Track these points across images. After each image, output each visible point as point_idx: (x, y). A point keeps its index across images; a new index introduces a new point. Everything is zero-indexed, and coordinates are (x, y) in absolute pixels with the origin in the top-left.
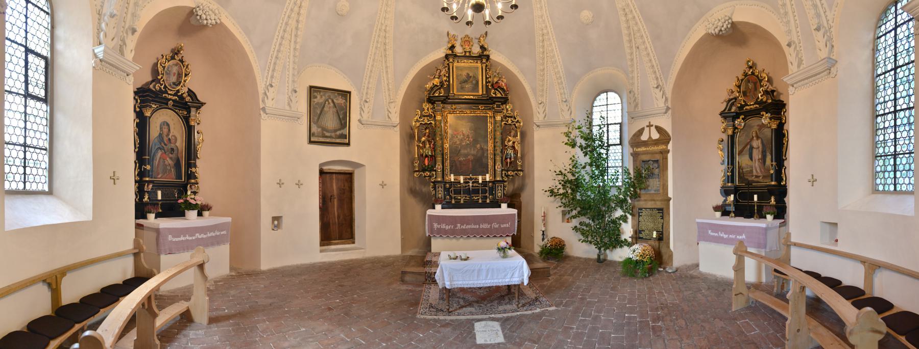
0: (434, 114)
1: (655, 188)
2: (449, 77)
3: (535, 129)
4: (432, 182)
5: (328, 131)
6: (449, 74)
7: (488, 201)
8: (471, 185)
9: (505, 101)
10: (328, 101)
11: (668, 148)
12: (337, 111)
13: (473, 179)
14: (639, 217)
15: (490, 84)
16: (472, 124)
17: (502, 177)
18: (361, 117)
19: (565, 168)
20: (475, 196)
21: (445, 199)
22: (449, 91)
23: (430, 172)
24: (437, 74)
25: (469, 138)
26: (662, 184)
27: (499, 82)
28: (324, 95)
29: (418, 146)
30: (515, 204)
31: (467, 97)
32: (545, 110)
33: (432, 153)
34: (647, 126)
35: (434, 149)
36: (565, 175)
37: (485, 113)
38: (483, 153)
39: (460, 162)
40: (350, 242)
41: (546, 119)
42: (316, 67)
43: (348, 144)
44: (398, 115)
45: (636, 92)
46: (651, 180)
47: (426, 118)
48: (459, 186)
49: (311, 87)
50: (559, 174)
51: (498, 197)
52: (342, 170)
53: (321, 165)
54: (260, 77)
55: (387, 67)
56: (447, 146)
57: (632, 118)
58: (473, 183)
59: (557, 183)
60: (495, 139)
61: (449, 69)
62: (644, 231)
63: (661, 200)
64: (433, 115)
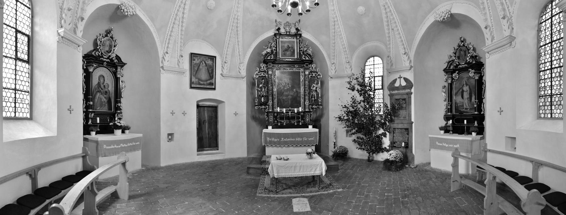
0: (267, 70)
2: (276, 47)
3: (329, 80)
4: (266, 112)
5: (202, 81)
7: (301, 124)
8: (290, 114)
9: (311, 62)
10: (202, 62)
12: (208, 68)
14: (393, 134)
15: (302, 52)
17: (309, 109)
19: (348, 104)
20: (293, 121)
21: (274, 122)
23: (265, 106)
24: (269, 46)
26: (407, 113)
28: (200, 59)
29: (258, 90)
32: (336, 68)
33: (266, 94)
34: (399, 78)
36: (348, 108)
37: (299, 70)
38: (298, 94)
39: (283, 99)
40: (216, 149)
43: (214, 89)
44: (245, 70)
45: (392, 57)
46: (401, 111)
47: (262, 73)
48: (283, 114)
49: (191, 54)
50: (344, 107)
51: (307, 121)
52: (210, 105)
53: (198, 102)
54: (160, 47)
55: (238, 41)
56: (275, 90)
57: (390, 73)
58: (291, 113)
61: (276, 42)
63: (407, 124)
64: (267, 71)
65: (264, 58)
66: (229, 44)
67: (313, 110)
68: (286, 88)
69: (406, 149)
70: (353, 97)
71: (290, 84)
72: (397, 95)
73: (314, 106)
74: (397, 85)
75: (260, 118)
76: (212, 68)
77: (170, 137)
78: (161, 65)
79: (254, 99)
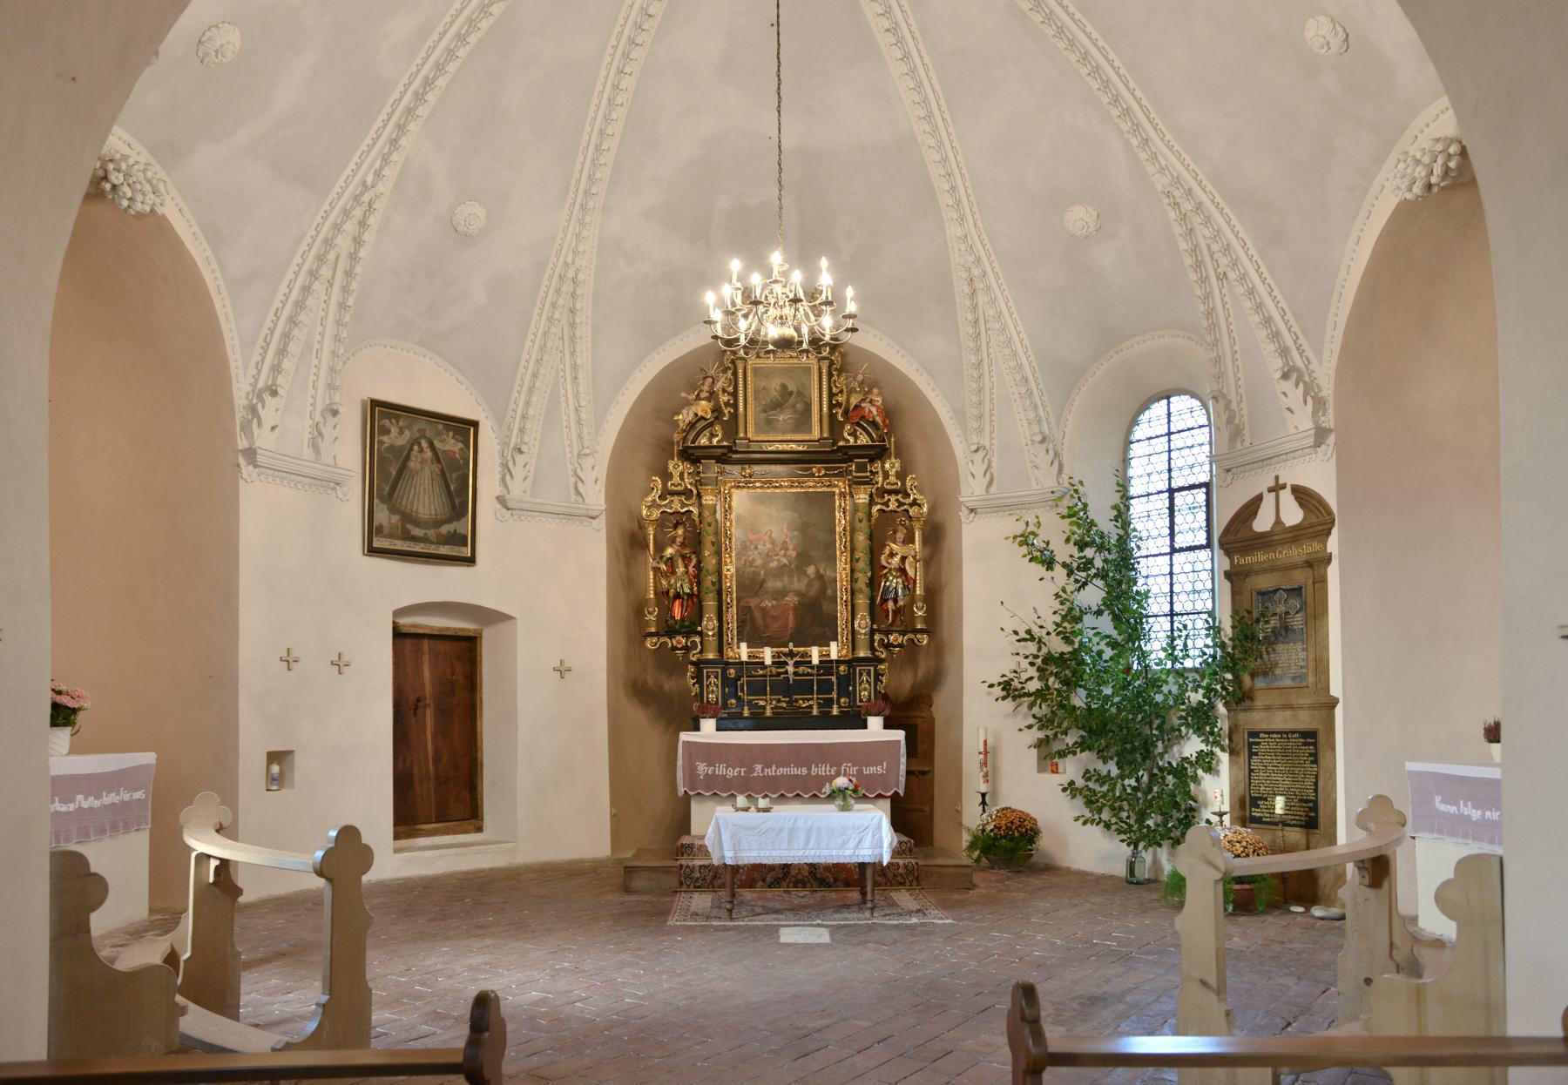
0: (697, 489)
1: (1293, 670)
2: (735, 394)
3: (963, 519)
4: (693, 663)
5: (417, 523)
6: (736, 388)
7: (835, 712)
8: (791, 669)
9: (878, 453)
10: (419, 444)
11: (1329, 551)
12: (442, 471)
13: (796, 655)
14: (1250, 758)
15: (840, 411)
16: (796, 515)
17: (873, 649)
18: (505, 492)
19: (1039, 622)
20: (803, 700)
21: (725, 706)
22: (737, 432)
23: (687, 638)
24: (706, 388)
25: (787, 549)
26: (1312, 657)
27: (863, 405)
28: (408, 427)
29: (656, 570)
30: (916, 725)
31: (781, 447)
32: (989, 466)
33: (692, 589)
34: (1270, 490)
35: (698, 578)
36: (1040, 641)
37: (828, 486)
38: (823, 589)
39: (763, 610)
40: (471, 827)
41: (993, 489)
42: (385, 346)
43: (471, 561)
44: (601, 485)
45: (1233, 396)
46: (1280, 647)
47: (676, 498)
48: (761, 672)
49: (375, 403)
50: (1024, 640)
51: (861, 701)
52: (448, 629)
53: (398, 613)
54: (237, 368)
55: (575, 367)
56: (730, 569)
57: (1228, 471)
58: (797, 664)
59: (1025, 664)
60: (852, 551)
61: (735, 374)
62: (1266, 799)
63: (1312, 707)
64: (695, 492)
65: (685, 439)
66: (535, 375)
67: (891, 653)
68: (774, 564)
69: (1308, 835)
70: (1061, 593)
71: (791, 547)
72: (1265, 571)
73: (892, 638)
74: (1262, 523)
75: (661, 687)
76: (461, 472)
77: (275, 769)
78: (243, 444)
79: (639, 610)
